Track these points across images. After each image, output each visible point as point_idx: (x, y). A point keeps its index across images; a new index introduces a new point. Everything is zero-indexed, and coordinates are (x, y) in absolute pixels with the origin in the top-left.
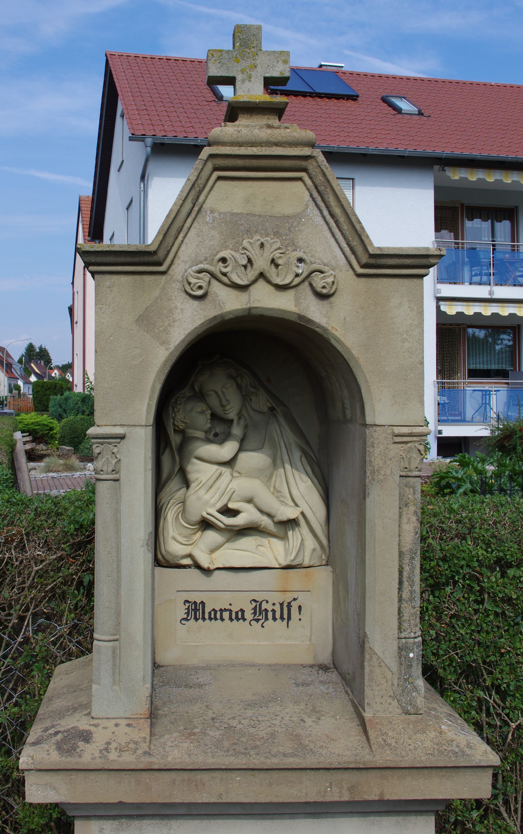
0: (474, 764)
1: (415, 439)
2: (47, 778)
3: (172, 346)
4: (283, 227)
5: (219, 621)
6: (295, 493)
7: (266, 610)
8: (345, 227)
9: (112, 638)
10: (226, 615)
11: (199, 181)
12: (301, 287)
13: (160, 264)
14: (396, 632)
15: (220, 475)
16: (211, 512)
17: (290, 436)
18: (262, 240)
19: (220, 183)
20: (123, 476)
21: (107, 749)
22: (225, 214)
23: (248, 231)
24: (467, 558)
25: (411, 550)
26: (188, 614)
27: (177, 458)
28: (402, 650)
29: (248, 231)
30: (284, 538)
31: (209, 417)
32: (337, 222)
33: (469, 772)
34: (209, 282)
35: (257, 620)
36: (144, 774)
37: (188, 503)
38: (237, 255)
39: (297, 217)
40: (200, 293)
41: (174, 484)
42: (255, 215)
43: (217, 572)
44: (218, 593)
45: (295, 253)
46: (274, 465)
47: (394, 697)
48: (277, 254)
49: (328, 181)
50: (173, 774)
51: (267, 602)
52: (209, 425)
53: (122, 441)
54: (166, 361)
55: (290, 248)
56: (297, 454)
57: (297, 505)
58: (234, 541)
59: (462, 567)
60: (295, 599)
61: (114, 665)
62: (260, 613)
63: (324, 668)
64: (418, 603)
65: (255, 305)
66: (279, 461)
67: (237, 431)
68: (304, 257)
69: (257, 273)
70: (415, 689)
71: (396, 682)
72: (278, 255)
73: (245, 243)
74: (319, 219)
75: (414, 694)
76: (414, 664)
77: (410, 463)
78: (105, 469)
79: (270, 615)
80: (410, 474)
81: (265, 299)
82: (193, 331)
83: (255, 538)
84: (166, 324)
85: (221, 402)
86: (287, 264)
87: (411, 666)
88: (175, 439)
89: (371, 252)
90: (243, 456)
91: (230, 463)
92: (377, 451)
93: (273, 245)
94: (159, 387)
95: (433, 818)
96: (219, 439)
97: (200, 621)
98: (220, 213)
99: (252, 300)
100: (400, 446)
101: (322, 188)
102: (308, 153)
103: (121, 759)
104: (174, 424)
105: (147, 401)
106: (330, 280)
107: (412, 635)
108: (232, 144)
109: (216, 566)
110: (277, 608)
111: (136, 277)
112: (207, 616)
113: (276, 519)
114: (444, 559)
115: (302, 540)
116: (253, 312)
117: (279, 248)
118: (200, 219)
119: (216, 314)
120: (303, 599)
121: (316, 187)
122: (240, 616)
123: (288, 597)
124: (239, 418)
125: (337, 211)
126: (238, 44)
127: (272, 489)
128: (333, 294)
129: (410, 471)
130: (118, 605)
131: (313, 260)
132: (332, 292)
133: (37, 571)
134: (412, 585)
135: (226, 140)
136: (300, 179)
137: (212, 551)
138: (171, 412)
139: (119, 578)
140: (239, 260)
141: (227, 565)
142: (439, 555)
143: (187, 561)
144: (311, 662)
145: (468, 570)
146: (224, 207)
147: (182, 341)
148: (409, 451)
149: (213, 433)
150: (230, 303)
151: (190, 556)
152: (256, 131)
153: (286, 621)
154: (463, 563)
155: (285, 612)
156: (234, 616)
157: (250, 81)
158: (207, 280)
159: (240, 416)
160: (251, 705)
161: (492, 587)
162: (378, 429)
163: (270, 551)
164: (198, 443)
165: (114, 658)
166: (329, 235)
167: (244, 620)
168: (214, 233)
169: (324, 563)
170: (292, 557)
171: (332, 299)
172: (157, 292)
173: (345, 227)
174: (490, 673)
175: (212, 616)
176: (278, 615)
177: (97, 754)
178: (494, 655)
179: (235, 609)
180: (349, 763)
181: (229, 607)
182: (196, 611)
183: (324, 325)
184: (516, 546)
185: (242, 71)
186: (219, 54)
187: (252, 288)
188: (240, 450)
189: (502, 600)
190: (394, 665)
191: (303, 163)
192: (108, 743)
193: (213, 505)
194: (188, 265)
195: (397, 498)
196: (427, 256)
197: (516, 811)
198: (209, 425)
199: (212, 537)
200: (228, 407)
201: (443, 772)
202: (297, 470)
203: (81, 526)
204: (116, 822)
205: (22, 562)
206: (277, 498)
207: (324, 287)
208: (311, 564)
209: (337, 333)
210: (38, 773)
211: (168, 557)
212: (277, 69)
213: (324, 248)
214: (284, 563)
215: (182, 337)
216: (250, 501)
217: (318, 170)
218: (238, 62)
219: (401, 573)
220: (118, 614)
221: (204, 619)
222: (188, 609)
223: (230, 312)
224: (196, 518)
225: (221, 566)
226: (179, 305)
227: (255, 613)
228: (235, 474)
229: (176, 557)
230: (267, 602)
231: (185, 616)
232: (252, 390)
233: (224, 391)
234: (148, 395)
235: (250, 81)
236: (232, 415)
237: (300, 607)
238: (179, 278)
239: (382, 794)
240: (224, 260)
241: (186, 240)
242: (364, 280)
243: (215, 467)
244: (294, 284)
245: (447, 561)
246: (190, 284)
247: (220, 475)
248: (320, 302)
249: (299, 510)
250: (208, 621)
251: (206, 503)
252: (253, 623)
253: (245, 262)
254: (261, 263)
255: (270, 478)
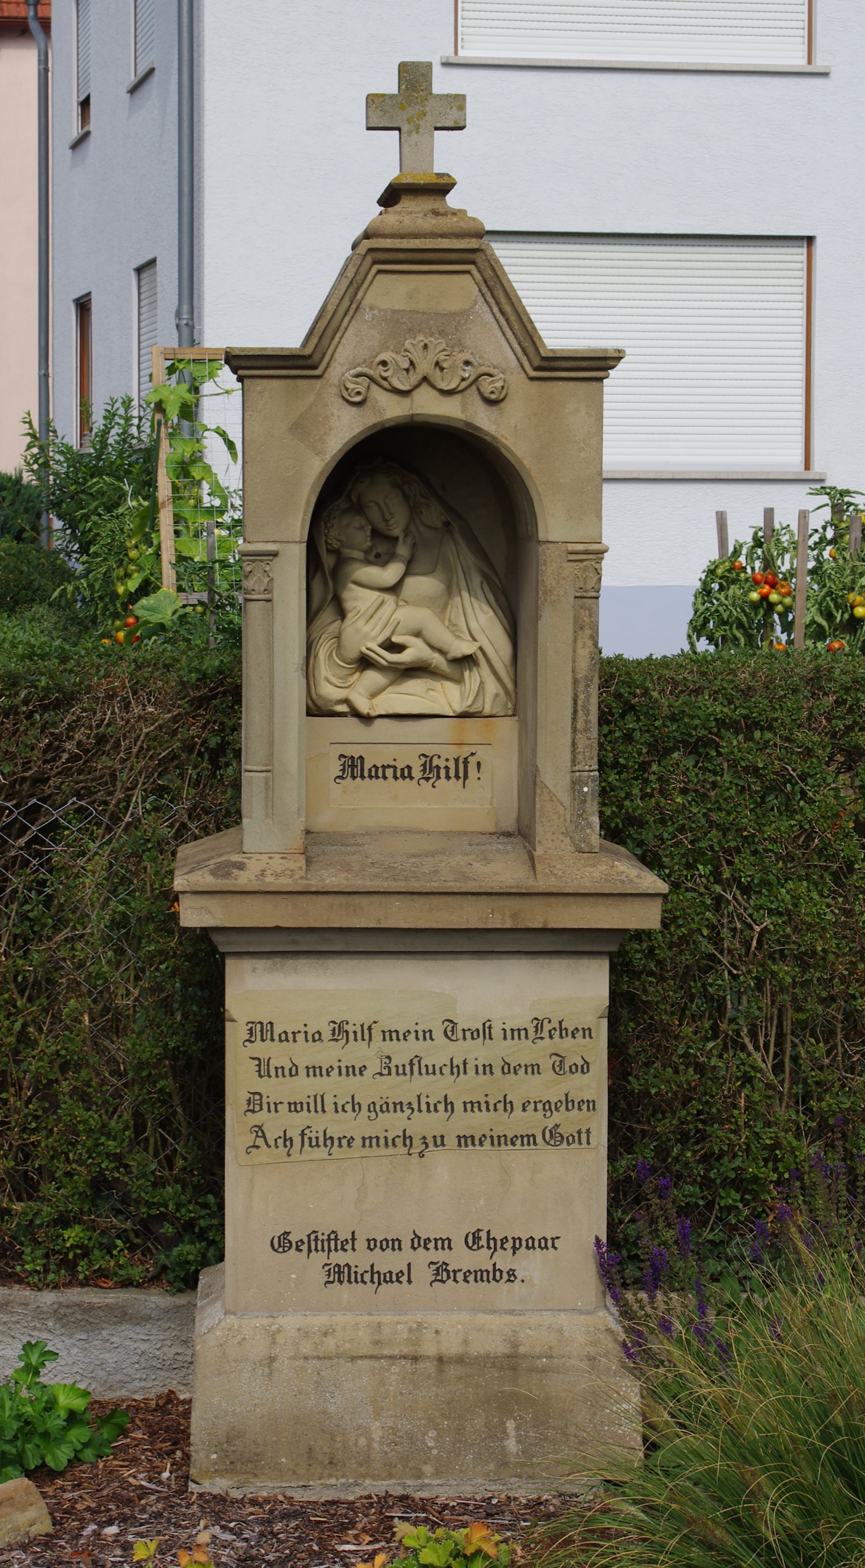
0: (641, 891)
1: (591, 556)
2: (202, 901)
3: (328, 457)
4: (449, 325)
5: (381, 780)
6: (473, 625)
7: (438, 767)
8: (516, 326)
9: (265, 768)
10: (389, 772)
11: (357, 278)
12: (469, 391)
13: (315, 367)
14: (569, 764)
15: (383, 602)
16: (371, 645)
17: (469, 558)
18: (426, 341)
19: (380, 277)
20: (276, 596)
21: (262, 875)
22: (385, 311)
23: (411, 330)
24: (703, 717)
25: (586, 677)
26: (343, 770)
27: (330, 583)
28: (576, 784)
29: (411, 330)
30: (459, 680)
31: (369, 533)
32: (507, 320)
33: (637, 900)
34: (369, 387)
35: (427, 779)
36: (301, 898)
37: (343, 637)
38: (398, 358)
39: (464, 314)
40: (358, 399)
41: (327, 615)
42: (418, 312)
43: (378, 721)
44: (382, 744)
45: (461, 355)
46: (450, 590)
47: (565, 834)
48: (442, 357)
49: (498, 277)
50: (330, 899)
51: (439, 757)
52: (369, 544)
53: (275, 559)
54: (322, 472)
55: (456, 349)
56: (477, 580)
57: (475, 640)
58: (399, 684)
59: (695, 728)
60: (473, 754)
61: (267, 797)
62: (431, 770)
63: (509, 835)
64: (594, 734)
65: (418, 412)
66: (455, 587)
67: (403, 550)
68: (472, 360)
69: (420, 377)
70: (590, 825)
71: (568, 818)
72: (443, 358)
73: (407, 345)
74: (488, 317)
75: (588, 831)
76: (589, 799)
77: (585, 583)
78: (256, 588)
79: (443, 773)
80: (585, 594)
81: (429, 405)
82: (351, 440)
83: (425, 680)
84: (322, 432)
85: (383, 516)
86: (453, 367)
87: (585, 801)
88: (328, 561)
89: (543, 355)
90: (410, 581)
91: (394, 589)
92: (550, 570)
93: (438, 344)
94: (314, 500)
95: (603, 966)
96: (381, 560)
97: (359, 779)
98: (380, 310)
99: (415, 406)
100: (574, 564)
101: (491, 283)
102: (476, 246)
103: (278, 882)
104: (327, 543)
105: (301, 515)
106: (499, 384)
107: (587, 768)
108: (393, 236)
109: (378, 713)
110: (451, 765)
111: (289, 381)
112: (366, 774)
113: (449, 656)
114: (673, 718)
115: (482, 683)
116: (416, 419)
117: (444, 350)
118: (358, 317)
119: (376, 421)
120: (482, 753)
121: (485, 282)
122: (406, 774)
123: (465, 751)
124: (406, 536)
125: (508, 309)
126: (403, 87)
127: (447, 623)
128: (503, 399)
129: (586, 591)
130: (271, 734)
131: (481, 361)
132: (501, 397)
133: (147, 734)
134: (587, 714)
135: (386, 232)
136: (468, 272)
137: (374, 695)
138: (323, 527)
139: (272, 705)
140: (400, 363)
141: (391, 712)
142: (666, 711)
143: (343, 708)
144: (492, 829)
145: (703, 732)
146: (385, 304)
147: (340, 451)
148: (585, 569)
149: (374, 553)
150: (391, 409)
151: (346, 701)
152: (420, 222)
153: (461, 780)
154: (697, 722)
155: (461, 771)
156: (398, 775)
157: (417, 132)
158: (366, 385)
159: (406, 532)
160: (414, 856)
161: (732, 753)
162: (551, 545)
163: (446, 697)
164: (355, 565)
165: (267, 789)
166: (500, 334)
167: (412, 778)
168: (373, 332)
169: (510, 712)
170: (469, 702)
171: (502, 405)
172: (312, 398)
173: (516, 326)
174: (730, 863)
175: (373, 774)
176: (452, 773)
177: (253, 878)
178: (735, 840)
179: (400, 765)
180: (510, 887)
181: (392, 763)
182: (353, 767)
183: (493, 433)
184: (766, 702)
185: (409, 121)
186: (381, 99)
187: (415, 394)
188: (406, 574)
189: (746, 769)
190: (566, 799)
191: (471, 256)
192: (264, 871)
193: (374, 639)
194: (345, 368)
195: (571, 621)
196: (605, 359)
197: (766, 1046)
198: (369, 544)
199: (373, 677)
200: (391, 522)
201: (610, 901)
202: (477, 598)
203: (205, 676)
204: (270, 962)
205: (128, 721)
206: (453, 632)
207: (492, 392)
208: (493, 713)
209: (506, 442)
210: (194, 896)
211: (320, 702)
212: (450, 117)
213: (494, 349)
214: (459, 708)
215: (340, 446)
216: (418, 634)
217: (487, 264)
218: (403, 109)
219: (575, 701)
220: (271, 744)
221: (363, 777)
222: (344, 765)
223: (390, 420)
224: (353, 654)
225: (383, 713)
226: (335, 411)
227: (424, 770)
228: (401, 603)
229: (330, 701)
230: (439, 757)
231: (340, 774)
232: (422, 500)
233: (388, 504)
234: (302, 509)
235: (417, 132)
236: (397, 531)
237: (479, 764)
238: (336, 382)
239: (545, 922)
240: (384, 363)
241: (343, 340)
242: (537, 383)
243: (376, 594)
244: (460, 388)
245: (677, 721)
246: (347, 389)
247: (383, 602)
248: (489, 408)
249: (477, 644)
250: (367, 779)
251: (366, 636)
252: (422, 782)
253: (406, 365)
254: (424, 367)
255: (444, 608)
